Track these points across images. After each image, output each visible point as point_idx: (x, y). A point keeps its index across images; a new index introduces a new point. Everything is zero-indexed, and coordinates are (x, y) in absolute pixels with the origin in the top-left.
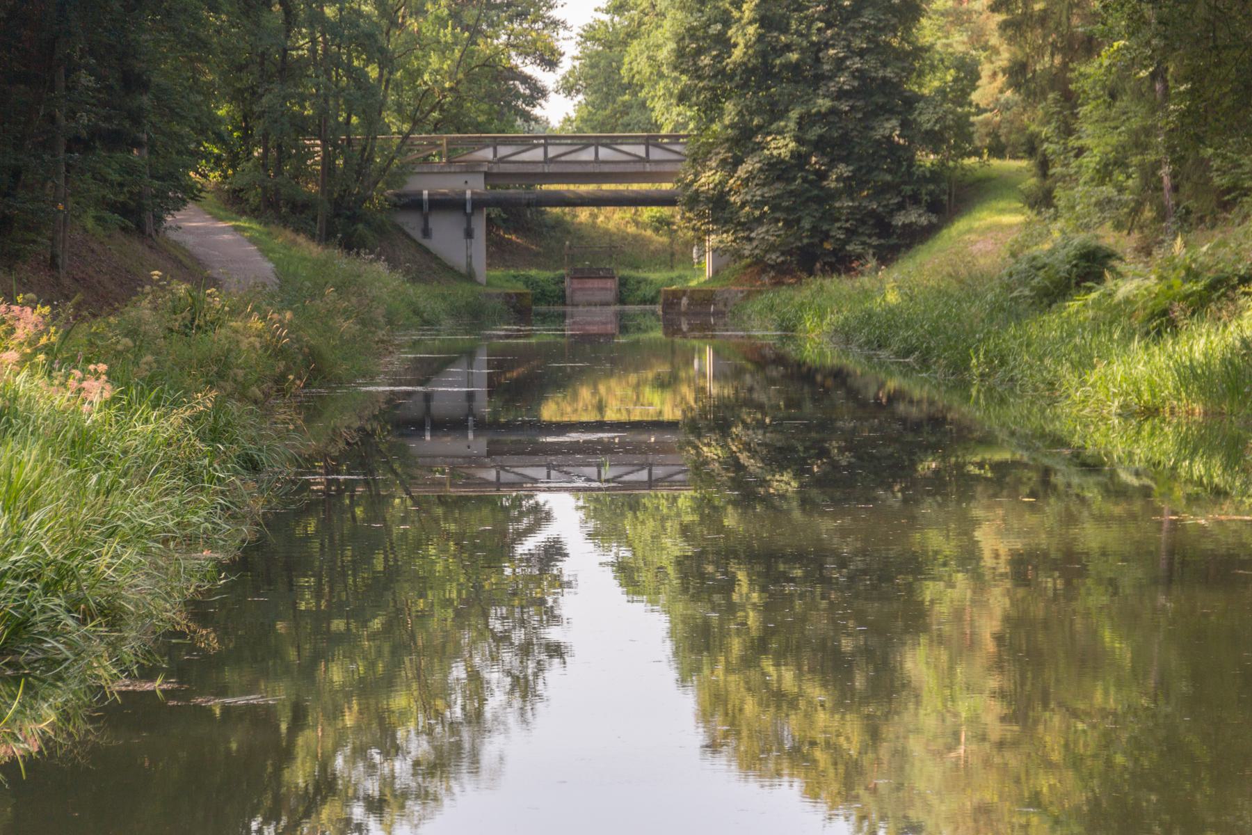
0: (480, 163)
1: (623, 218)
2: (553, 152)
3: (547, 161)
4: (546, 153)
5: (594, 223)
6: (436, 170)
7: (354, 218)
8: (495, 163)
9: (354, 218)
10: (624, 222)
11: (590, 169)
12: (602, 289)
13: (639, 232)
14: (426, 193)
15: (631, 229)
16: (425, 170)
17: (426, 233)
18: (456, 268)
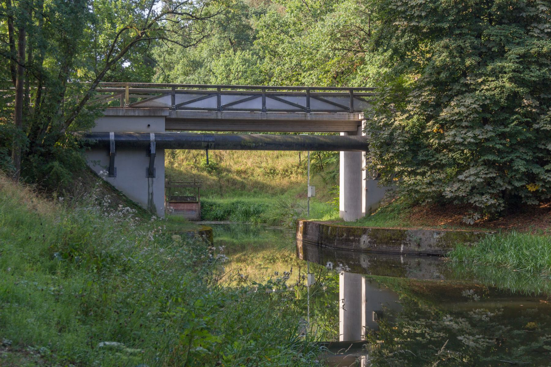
0: (162, 109)
1: (189, 165)
2: (225, 100)
3: (220, 109)
4: (219, 102)
5: (172, 168)
6: (121, 114)
7: (48, 156)
8: (174, 109)
9: (48, 156)
10: (189, 167)
11: (258, 116)
12: (190, 210)
13: (199, 173)
14: (112, 134)
15: (195, 172)
16: (111, 114)
17: (112, 171)
18: (139, 205)
